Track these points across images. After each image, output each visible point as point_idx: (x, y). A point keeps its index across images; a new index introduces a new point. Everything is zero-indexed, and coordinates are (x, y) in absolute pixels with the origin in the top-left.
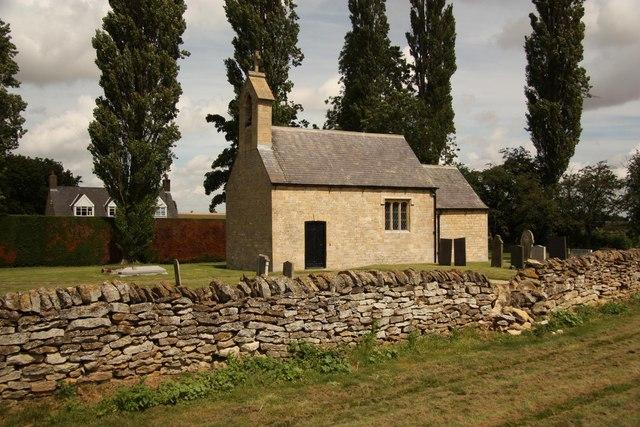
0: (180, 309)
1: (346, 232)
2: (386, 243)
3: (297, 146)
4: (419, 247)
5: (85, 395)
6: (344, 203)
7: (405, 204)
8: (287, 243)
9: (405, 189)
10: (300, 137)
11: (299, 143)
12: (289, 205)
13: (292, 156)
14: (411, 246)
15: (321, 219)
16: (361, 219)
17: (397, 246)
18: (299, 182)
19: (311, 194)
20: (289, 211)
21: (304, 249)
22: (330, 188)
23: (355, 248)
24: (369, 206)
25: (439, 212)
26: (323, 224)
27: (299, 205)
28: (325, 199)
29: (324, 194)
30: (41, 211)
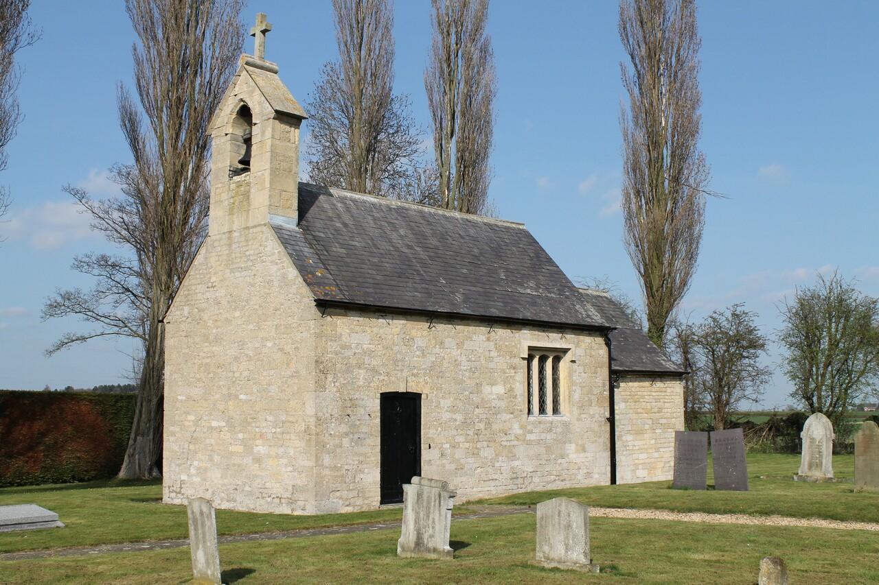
0: (144, 251)
1: (459, 417)
2: (529, 443)
3: (345, 225)
4: (584, 450)
5: (190, 292)
6: (455, 352)
7: (558, 354)
8: (346, 442)
9: (561, 327)
10: (348, 209)
11: (346, 218)
12: (350, 353)
13: (342, 246)
14: (571, 448)
15: (413, 388)
16: (486, 389)
17: (548, 449)
18: (370, 301)
19: (395, 327)
20: (349, 369)
21: (378, 458)
22: (431, 316)
23: (475, 453)
24: (500, 362)
25: (616, 376)
26: (382, 394)
27: (370, 353)
28: (420, 342)
29: (418, 330)
30: (131, 398)
